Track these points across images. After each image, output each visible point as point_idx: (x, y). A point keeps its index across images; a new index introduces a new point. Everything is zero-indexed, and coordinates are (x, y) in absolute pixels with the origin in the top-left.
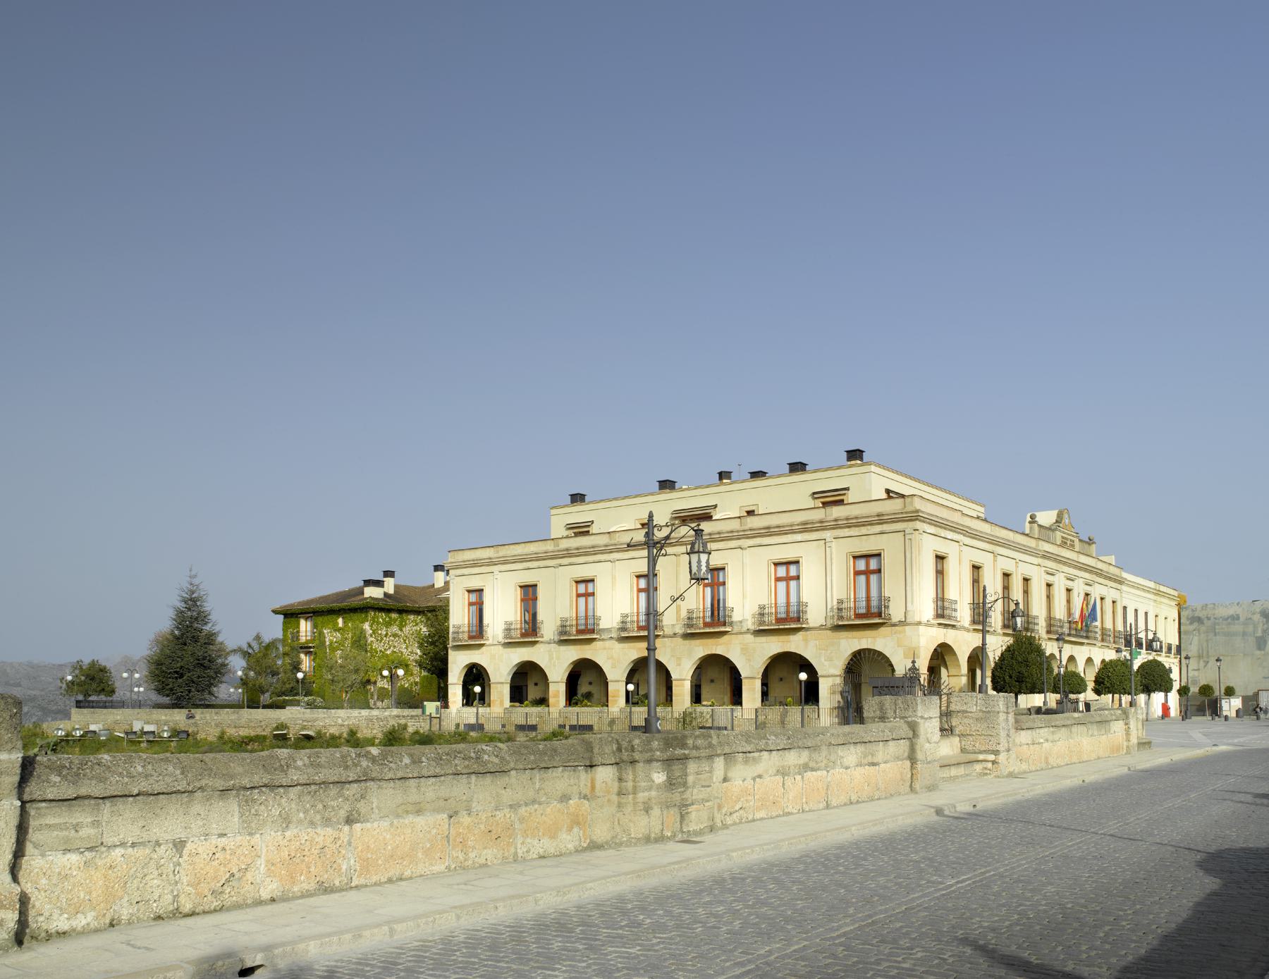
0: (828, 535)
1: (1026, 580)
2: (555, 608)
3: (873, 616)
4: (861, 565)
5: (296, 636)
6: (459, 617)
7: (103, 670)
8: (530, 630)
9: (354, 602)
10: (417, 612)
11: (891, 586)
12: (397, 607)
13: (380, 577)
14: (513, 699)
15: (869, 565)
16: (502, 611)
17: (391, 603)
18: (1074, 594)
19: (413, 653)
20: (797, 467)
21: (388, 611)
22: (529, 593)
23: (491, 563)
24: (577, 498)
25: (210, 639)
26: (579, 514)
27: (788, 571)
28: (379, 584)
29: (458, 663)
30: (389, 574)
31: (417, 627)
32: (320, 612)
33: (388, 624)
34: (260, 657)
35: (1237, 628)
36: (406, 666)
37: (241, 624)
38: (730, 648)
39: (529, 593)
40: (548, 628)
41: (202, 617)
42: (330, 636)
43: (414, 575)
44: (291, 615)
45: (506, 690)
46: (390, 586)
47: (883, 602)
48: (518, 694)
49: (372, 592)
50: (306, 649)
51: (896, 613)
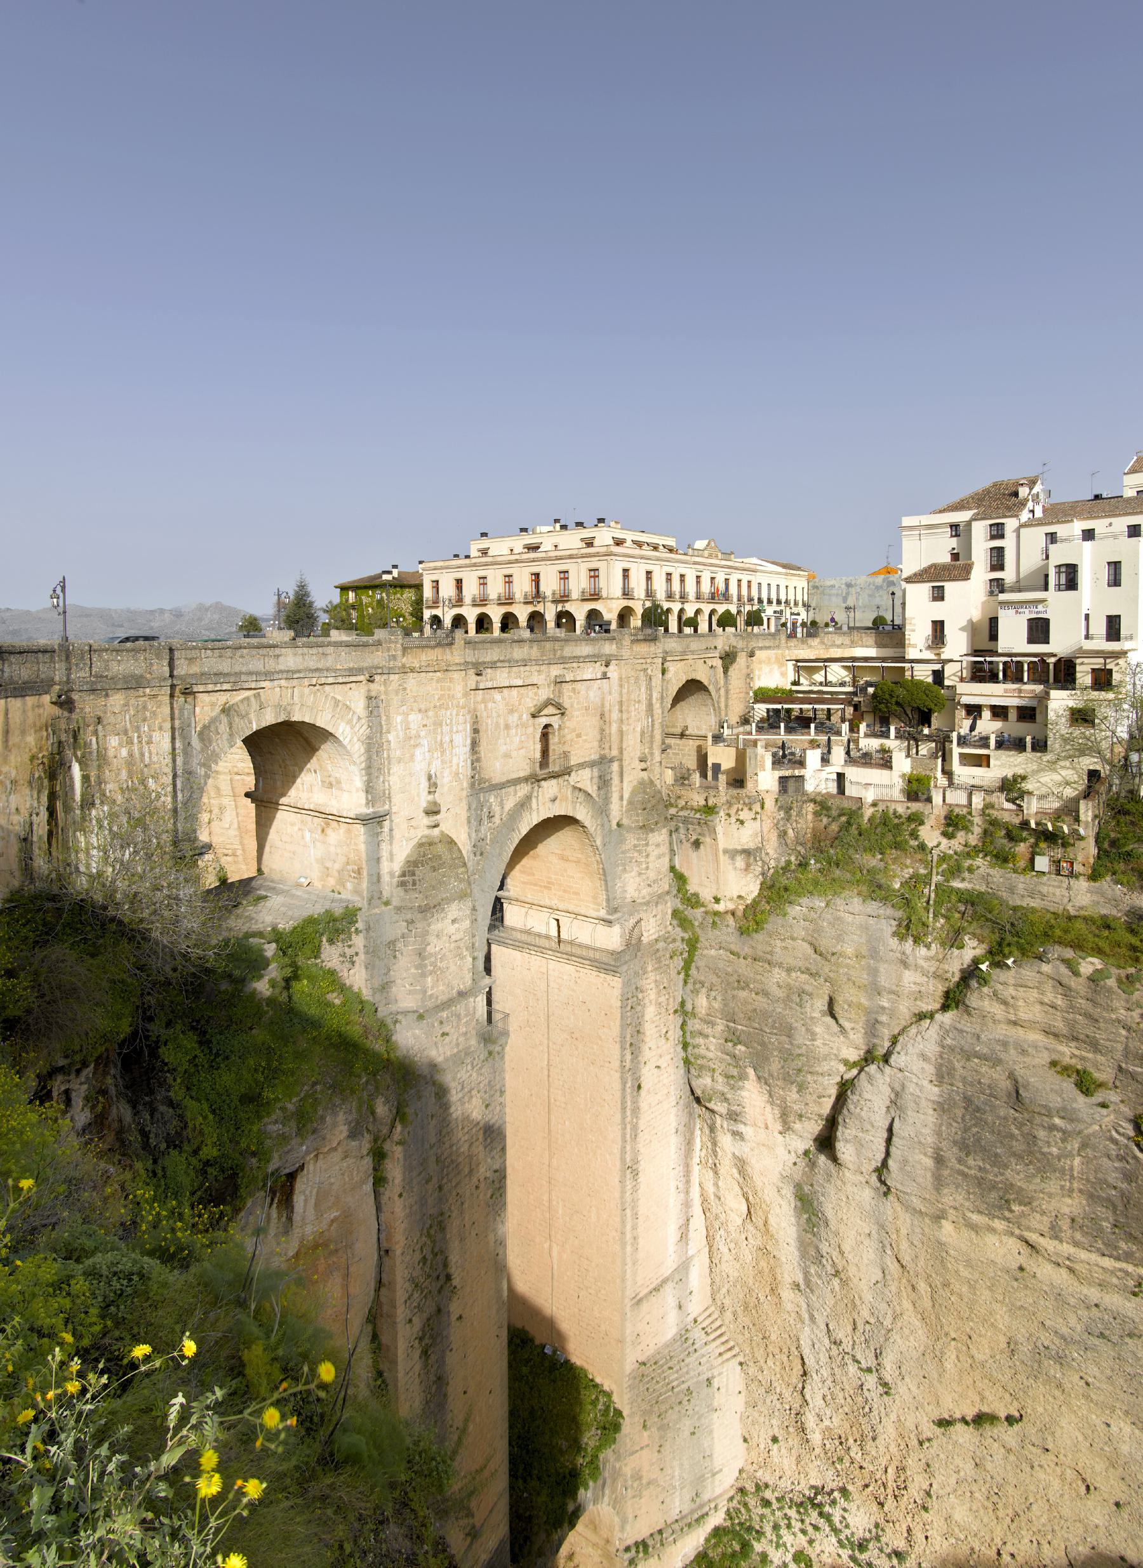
0: (579, 560)
1: (682, 576)
2: (471, 590)
3: (595, 596)
4: (592, 573)
5: (347, 600)
6: (428, 593)
7: (255, 619)
8: (460, 601)
9: (377, 582)
10: (410, 587)
11: (602, 582)
12: (399, 585)
13: (390, 569)
14: (1046, 622)
15: (594, 573)
16: (447, 590)
17: (396, 582)
18: (703, 580)
19: (407, 609)
20: (580, 524)
21: (395, 587)
22: (459, 582)
23: (442, 568)
24: (484, 535)
25: (311, 604)
26: (484, 543)
27: (564, 575)
28: (389, 572)
29: (427, 614)
30: (395, 567)
31: (409, 595)
32: (359, 587)
33: (395, 594)
34: (331, 610)
35: (834, 591)
36: (404, 617)
37: (324, 596)
38: (568, 607)
39: (459, 582)
40: (468, 599)
41: (307, 594)
42: (365, 599)
43: (408, 566)
44: (344, 589)
45: (474, 626)
46: (395, 573)
47: (600, 590)
48: (504, 627)
49: (385, 577)
50: (353, 607)
51: (604, 594)
